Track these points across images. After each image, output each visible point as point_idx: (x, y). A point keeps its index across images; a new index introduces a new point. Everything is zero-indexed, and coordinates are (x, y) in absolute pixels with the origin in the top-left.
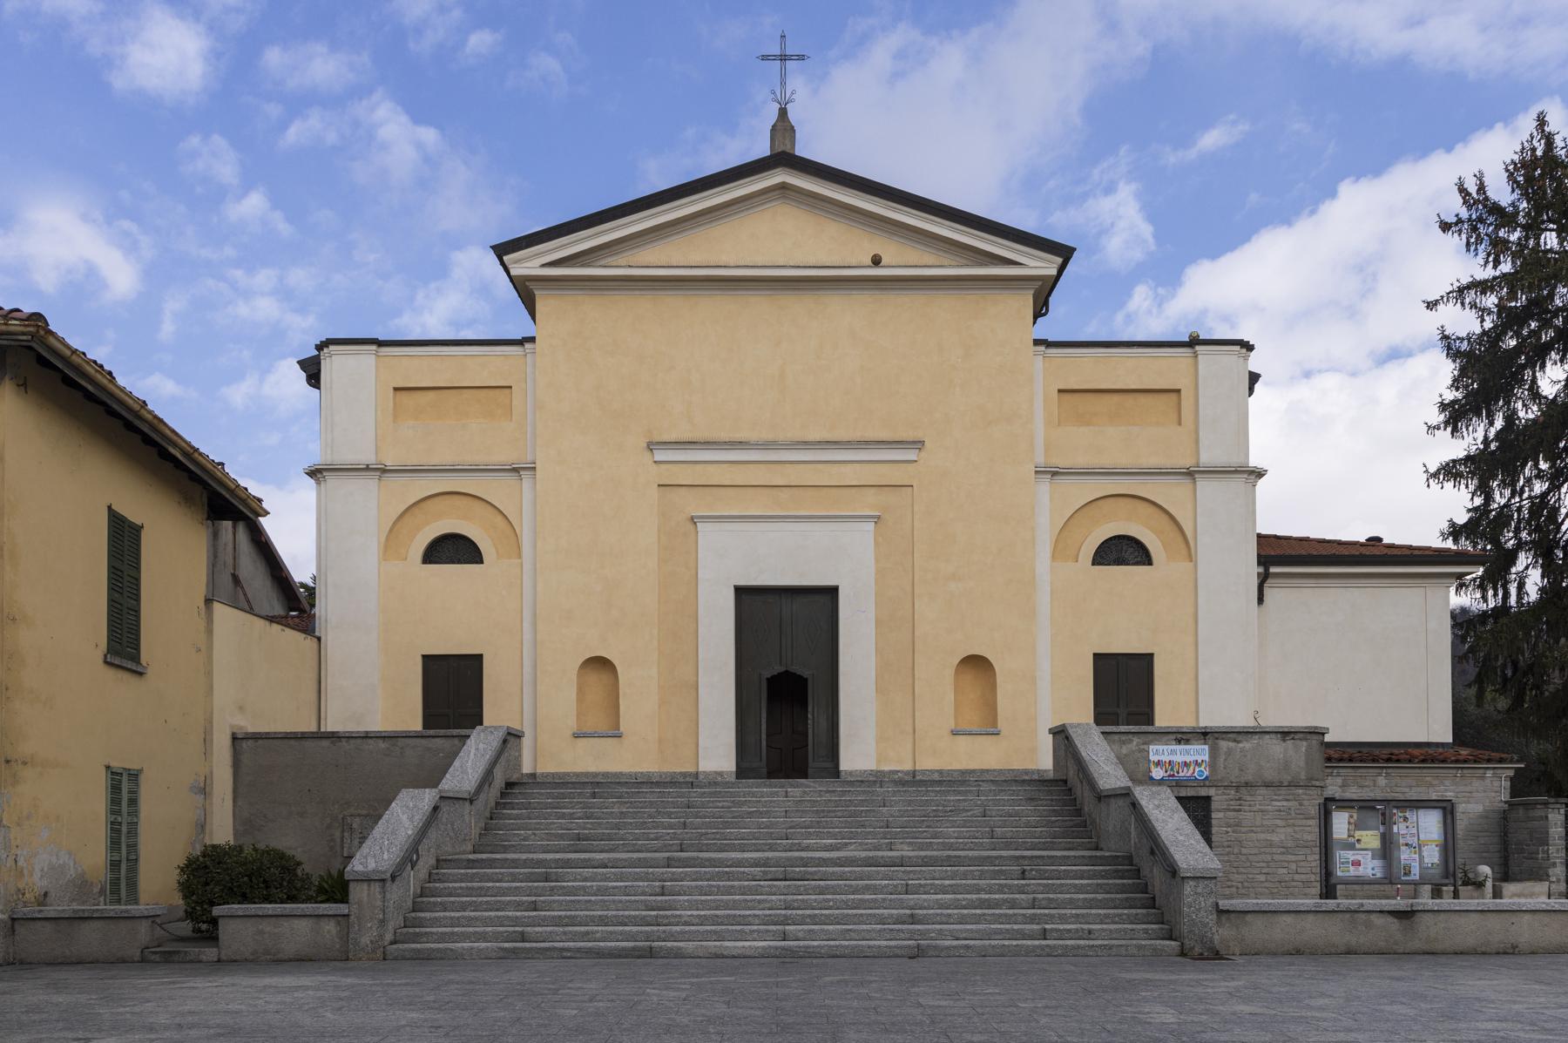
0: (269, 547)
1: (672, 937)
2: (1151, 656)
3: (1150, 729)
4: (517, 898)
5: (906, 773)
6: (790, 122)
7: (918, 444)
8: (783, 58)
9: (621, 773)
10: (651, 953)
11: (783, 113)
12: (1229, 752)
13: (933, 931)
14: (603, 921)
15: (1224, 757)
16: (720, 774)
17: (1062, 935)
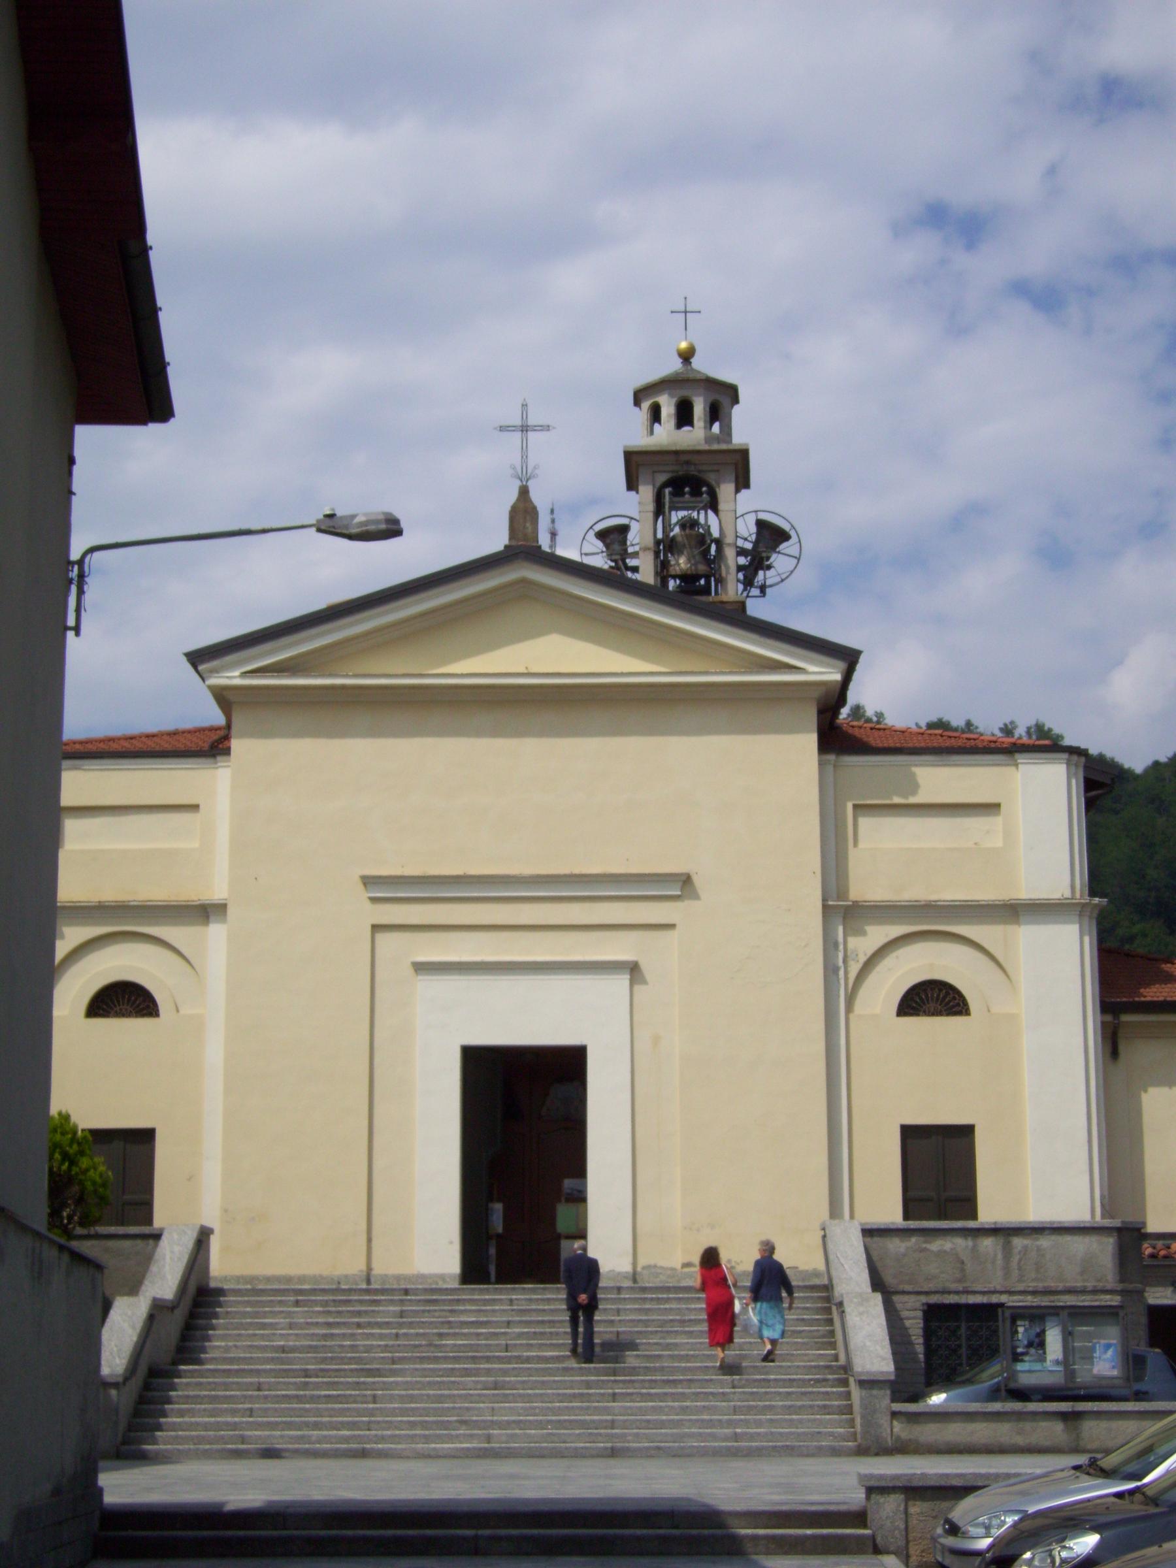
0: (688, 1554)
1: (383, 1439)
2: (965, 1132)
3: (971, 1224)
4: (234, 1406)
5: (624, 1276)
6: (531, 501)
7: (685, 884)
8: (525, 429)
9: (321, 1276)
10: (363, 1454)
11: (524, 492)
12: (1025, 1249)
13: (630, 1434)
14: (316, 1426)
15: (1018, 1257)
16: (442, 1277)
17: (752, 1437)
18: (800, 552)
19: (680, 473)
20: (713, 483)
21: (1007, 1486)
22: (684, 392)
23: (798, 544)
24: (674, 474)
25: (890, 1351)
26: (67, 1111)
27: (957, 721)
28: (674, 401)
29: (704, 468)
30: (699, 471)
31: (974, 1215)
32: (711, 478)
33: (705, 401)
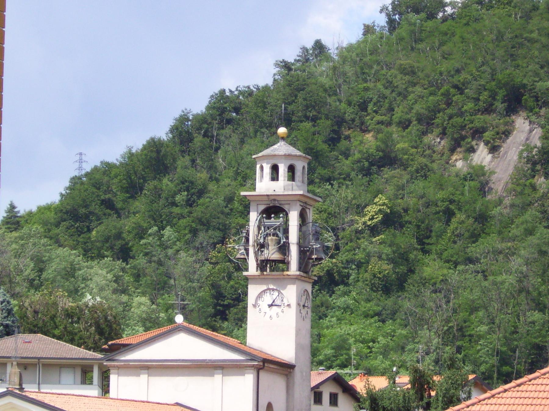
18: (112, 399)
19: (271, 205)
20: (287, 210)
21: (262, 176)
22: (275, 162)
23: (145, 400)
24: (268, 206)
25: (292, 285)
26: (102, 162)
27: (145, 143)
28: (269, 166)
29: (283, 202)
30: (280, 204)
31: (254, 189)
32: (286, 207)
33: (285, 165)
